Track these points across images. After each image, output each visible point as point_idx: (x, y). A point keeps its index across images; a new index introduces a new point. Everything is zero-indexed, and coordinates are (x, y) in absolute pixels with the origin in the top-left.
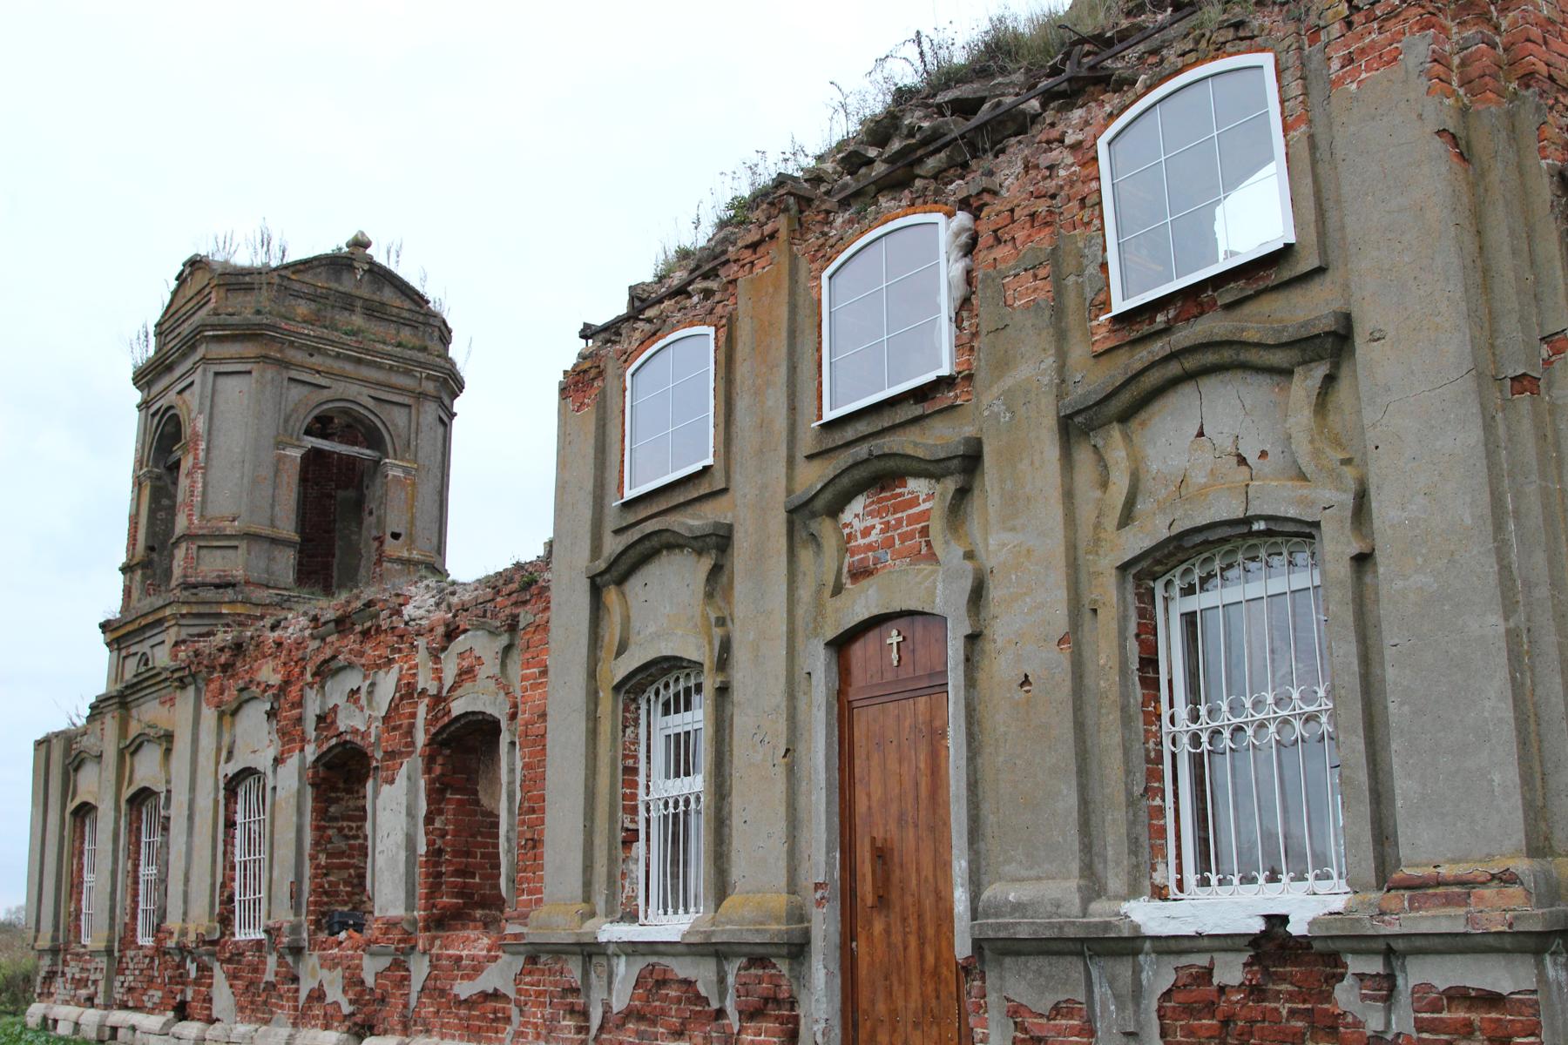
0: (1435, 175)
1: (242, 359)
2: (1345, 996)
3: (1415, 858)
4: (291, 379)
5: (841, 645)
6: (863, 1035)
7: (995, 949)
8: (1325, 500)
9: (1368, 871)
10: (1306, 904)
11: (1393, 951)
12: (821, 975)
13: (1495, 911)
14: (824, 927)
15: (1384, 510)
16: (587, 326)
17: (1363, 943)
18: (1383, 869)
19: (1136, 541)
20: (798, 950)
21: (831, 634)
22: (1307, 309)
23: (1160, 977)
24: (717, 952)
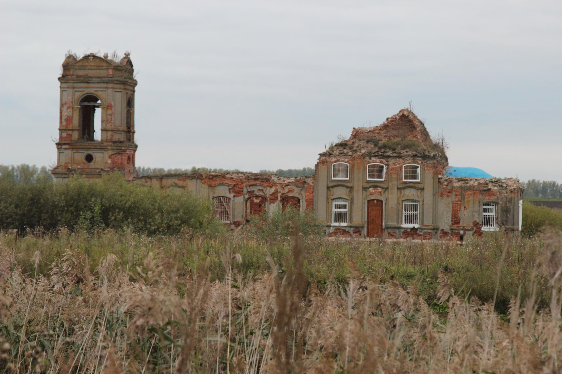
0: (432, 180)
1: (120, 89)
2: (418, 232)
3: (425, 223)
4: (115, 91)
5: (368, 201)
6: (558, 199)
7: (387, 228)
8: (421, 200)
9: (421, 223)
10: (416, 226)
11: (423, 229)
12: (366, 229)
13: (430, 227)
14: (366, 225)
15: (425, 201)
16: (122, 75)
17: (420, 229)
18: (422, 224)
19: (404, 199)
20: (363, 227)
21: (368, 199)
22: (421, 186)
23: (403, 230)
24: (351, 227)
